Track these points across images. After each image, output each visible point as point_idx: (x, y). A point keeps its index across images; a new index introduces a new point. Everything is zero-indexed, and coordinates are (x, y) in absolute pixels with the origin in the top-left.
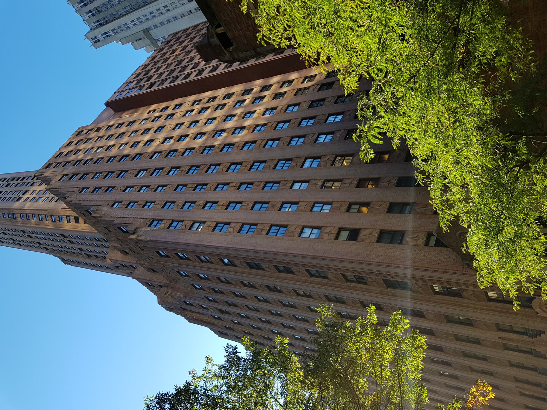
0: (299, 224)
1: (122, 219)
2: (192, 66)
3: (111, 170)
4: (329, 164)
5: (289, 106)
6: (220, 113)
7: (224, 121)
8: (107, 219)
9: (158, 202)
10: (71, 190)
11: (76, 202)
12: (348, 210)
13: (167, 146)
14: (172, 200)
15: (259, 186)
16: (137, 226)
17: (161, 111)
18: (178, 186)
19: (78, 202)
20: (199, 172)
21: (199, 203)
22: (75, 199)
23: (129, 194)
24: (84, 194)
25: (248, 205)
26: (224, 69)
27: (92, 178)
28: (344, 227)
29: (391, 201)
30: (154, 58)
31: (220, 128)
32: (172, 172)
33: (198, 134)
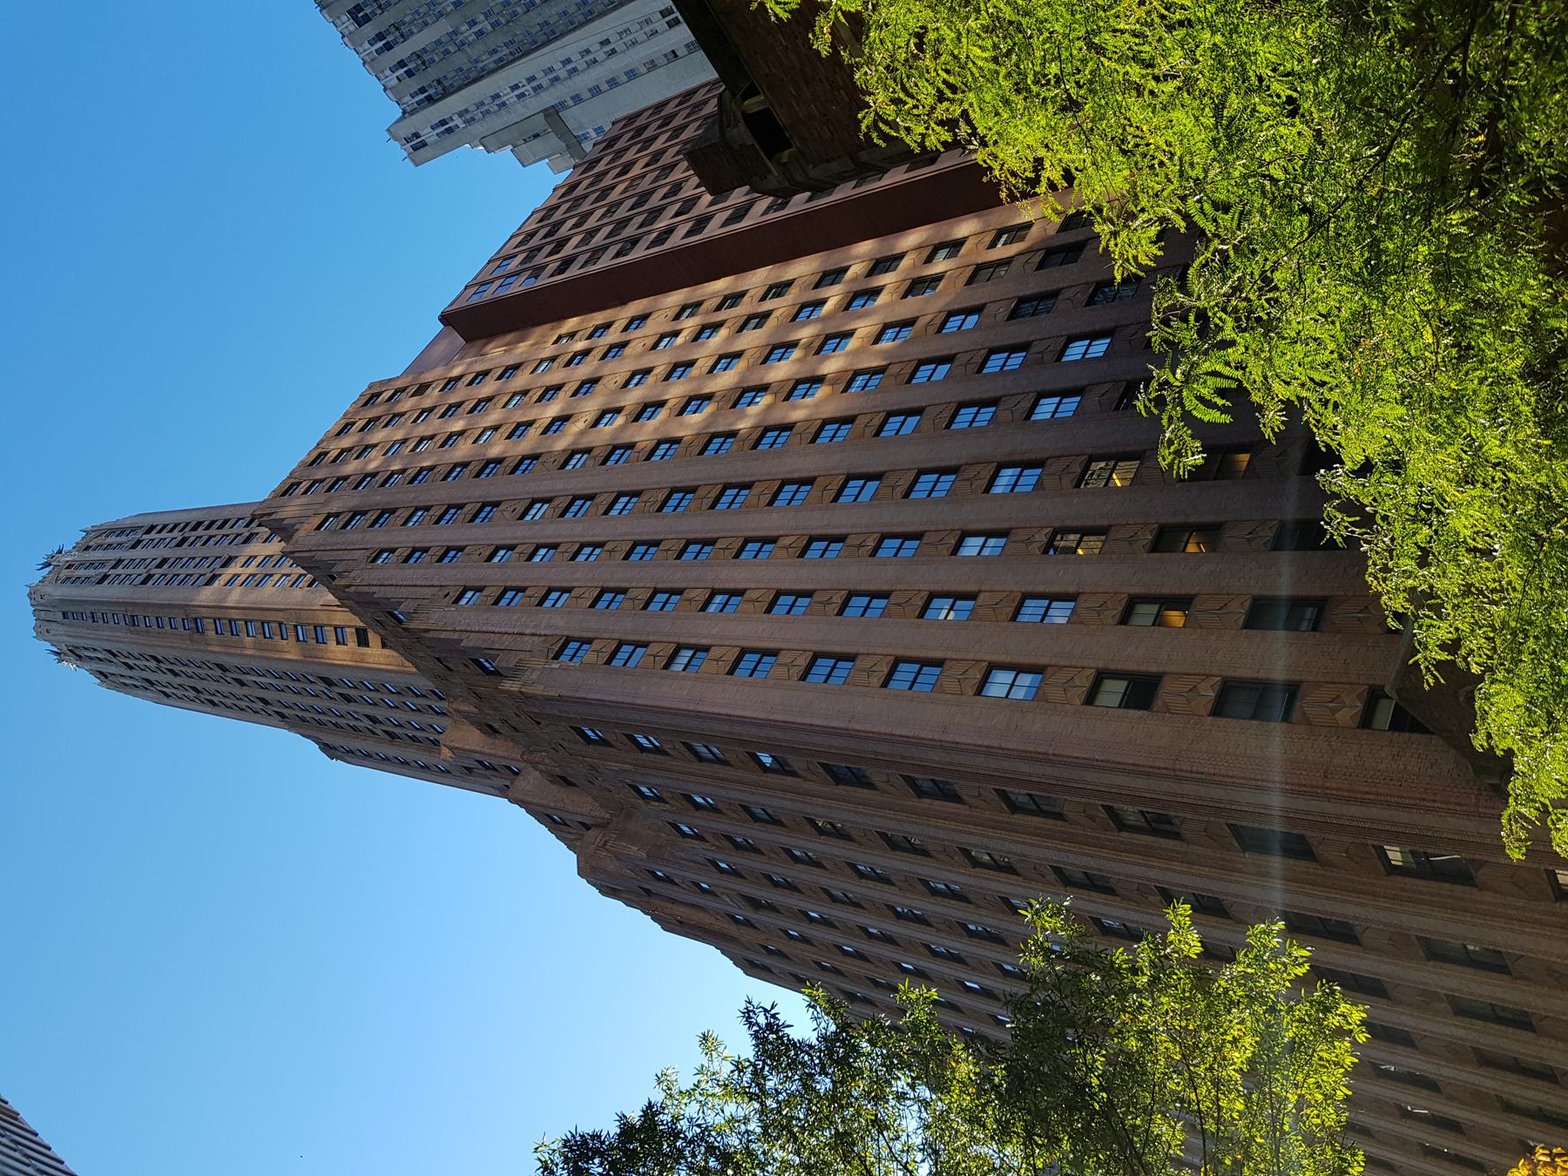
0: (978, 657)
4: (1067, 481)
5: (951, 314)
6: (752, 339)
7: (764, 362)
8: (443, 635)
12: (1125, 619)
13: (608, 431)
15: (860, 546)
16: (522, 655)
17: (589, 337)
19: (365, 589)
24: (381, 567)
25: (828, 602)
28: (1112, 667)
29: (1255, 592)
30: (573, 187)
31: (754, 380)
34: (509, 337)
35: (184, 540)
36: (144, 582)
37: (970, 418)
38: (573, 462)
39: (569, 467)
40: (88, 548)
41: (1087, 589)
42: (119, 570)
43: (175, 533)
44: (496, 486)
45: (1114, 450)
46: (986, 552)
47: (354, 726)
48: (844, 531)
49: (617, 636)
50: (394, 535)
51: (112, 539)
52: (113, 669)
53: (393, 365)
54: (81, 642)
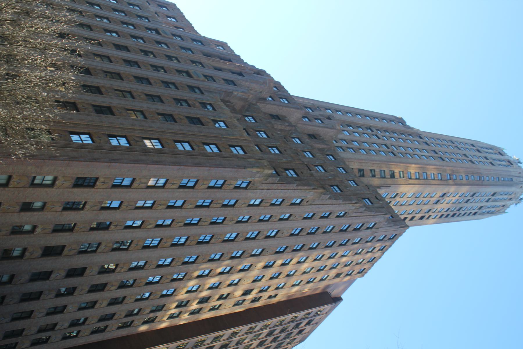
0: (58, 190)
1: (288, 188)
2: (260, 337)
3: (313, 235)
4: (30, 249)
6: (225, 291)
8: (306, 187)
9: (243, 206)
11: (350, 202)
15: (117, 225)
16: (266, 182)
17: (244, 300)
19: (347, 202)
20: (197, 238)
21: (190, 206)
23: (340, 211)
25: (127, 206)
26: (256, 326)
31: (224, 276)
34: (318, 292)
35: (459, 210)
36: (475, 194)
40: (504, 206)
41: (16, 214)
42: (487, 198)
43: (463, 213)
45: (13, 261)
46: (110, 202)
47: (388, 132)
48: (125, 231)
49: (222, 190)
51: (493, 209)
52: (494, 156)
53: (359, 282)
54: (504, 168)
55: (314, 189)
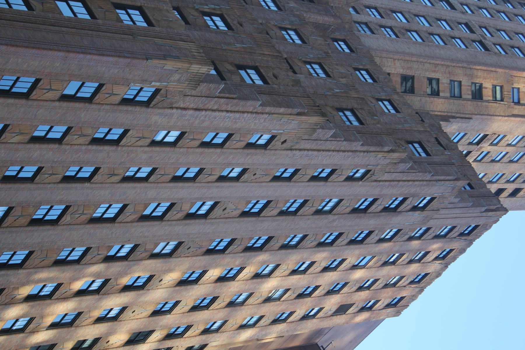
1: (241, 109)
3: (291, 218)
8: (282, 110)
9: (140, 143)
10: (399, 176)
13: (139, 272)
14: (101, 148)
16: (194, 93)
18: (326, 179)
19: (372, 149)
22: (380, 155)
24: (327, 166)
27: (340, 201)
31: (88, 300)
32: (296, 205)
33: (142, 287)
37: (15, 257)
38: (391, 233)
39: (395, 230)
44: (256, 231)
50: (361, 193)
55: (299, 114)
